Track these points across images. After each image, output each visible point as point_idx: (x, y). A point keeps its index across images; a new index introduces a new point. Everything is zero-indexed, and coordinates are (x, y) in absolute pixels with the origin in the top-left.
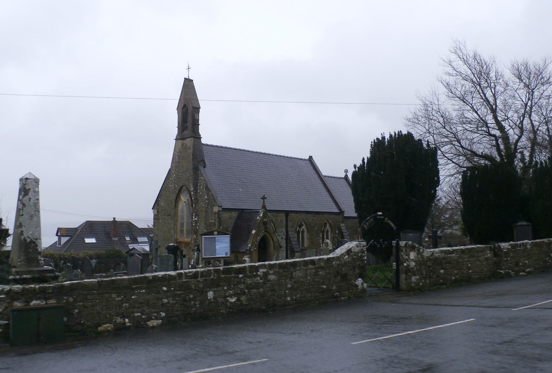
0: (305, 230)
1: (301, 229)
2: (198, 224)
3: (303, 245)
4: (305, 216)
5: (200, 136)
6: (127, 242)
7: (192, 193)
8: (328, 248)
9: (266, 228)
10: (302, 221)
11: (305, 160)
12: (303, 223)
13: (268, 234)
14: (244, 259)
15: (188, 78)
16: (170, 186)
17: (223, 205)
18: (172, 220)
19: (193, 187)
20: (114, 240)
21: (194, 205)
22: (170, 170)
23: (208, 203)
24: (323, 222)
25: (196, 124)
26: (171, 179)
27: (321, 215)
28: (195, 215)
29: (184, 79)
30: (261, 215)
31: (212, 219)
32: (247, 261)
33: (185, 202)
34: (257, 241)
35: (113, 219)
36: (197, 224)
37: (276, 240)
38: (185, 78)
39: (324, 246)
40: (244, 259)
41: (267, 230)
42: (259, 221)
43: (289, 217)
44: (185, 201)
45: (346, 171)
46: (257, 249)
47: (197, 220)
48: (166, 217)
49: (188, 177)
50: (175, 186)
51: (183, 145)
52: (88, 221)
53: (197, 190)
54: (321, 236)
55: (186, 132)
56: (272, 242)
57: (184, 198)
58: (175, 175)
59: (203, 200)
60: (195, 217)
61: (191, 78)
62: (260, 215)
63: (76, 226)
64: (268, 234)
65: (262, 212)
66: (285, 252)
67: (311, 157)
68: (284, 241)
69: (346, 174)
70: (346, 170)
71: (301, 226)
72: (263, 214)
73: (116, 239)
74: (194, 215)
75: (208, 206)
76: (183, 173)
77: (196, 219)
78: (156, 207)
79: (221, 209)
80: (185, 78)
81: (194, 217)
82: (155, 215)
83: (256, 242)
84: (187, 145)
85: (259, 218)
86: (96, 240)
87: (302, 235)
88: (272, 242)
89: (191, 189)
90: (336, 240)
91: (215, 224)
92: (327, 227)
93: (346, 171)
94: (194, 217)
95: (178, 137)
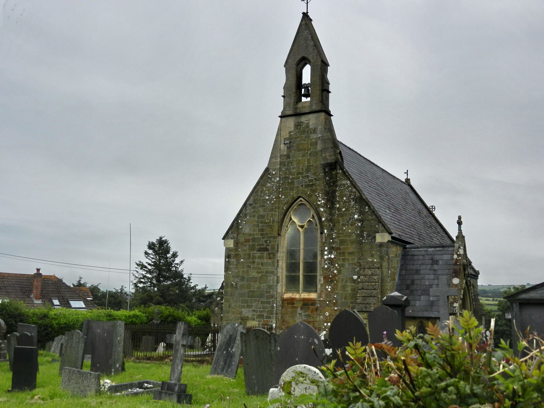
2: (337, 265)
6: (55, 307)
7: (322, 210)
18: (270, 258)
20: (36, 304)
22: (267, 170)
26: (269, 185)
35: (35, 272)
47: (334, 258)
53: (333, 204)
58: (278, 179)
60: (330, 253)
70: (432, 206)
73: (39, 302)
74: (326, 248)
75: (362, 232)
76: (299, 173)
81: (326, 253)
94: (326, 253)
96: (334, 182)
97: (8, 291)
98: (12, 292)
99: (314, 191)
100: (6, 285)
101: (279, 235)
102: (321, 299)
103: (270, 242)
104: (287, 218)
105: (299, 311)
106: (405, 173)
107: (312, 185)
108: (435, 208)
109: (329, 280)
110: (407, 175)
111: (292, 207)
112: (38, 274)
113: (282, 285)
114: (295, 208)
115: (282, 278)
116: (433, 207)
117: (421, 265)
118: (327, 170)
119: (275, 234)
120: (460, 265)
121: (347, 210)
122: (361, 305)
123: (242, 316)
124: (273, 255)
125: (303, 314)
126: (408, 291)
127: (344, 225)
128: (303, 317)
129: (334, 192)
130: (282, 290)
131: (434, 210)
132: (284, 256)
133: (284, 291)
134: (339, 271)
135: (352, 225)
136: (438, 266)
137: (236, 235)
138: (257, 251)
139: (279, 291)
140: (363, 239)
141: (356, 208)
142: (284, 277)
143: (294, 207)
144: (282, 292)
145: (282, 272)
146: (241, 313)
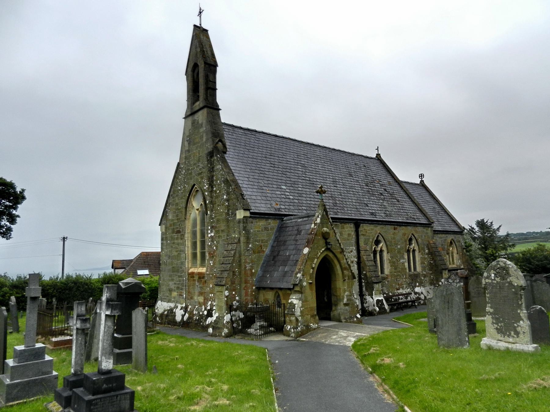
0: (384, 249)
1: (377, 247)
3: (382, 272)
4: (383, 227)
5: (218, 106)
8: (510, 283)
9: (327, 243)
10: (378, 235)
11: (372, 158)
12: (380, 238)
13: (331, 255)
14: (290, 301)
15: (199, 25)
16: (179, 188)
17: (252, 208)
19: (207, 184)
21: (209, 212)
22: (179, 164)
23: (228, 206)
24: (408, 237)
25: (211, 89)
27: (404, 227)
28: (210, 228)
29: (193, 27)
30: (319, 220)
31: (235, 232)
32: (296, 306)
33: (198, 210)
34: (313, 268)
36: (214, 243)
37: (347, 266)
38: (195, 26)
39: (493, 275)
40: (290, 301)
41: (329, 247)
42: (315, 231)
43: (360, 229)
44: (198, 208)
45: (421, 176)
46: (314, 283)
48: (175, 234)
49: (200, 169)
50: (184, 187)
51: (193, 123)
52: (143, 252)
53: (212, 188)
54: (406, 257)
55: (198, 104)
56: (338, 267)
57: (196, 203)
59: (220, 202)
60: (211, 232)
61: (204, 26)
62: (316, 220)
63: (132, 258)
64: (331, 255)
65: (320, 216)
66: (358, 284)
67: (378, 155)
68: (356, 266)
69: (422, 179)
70: (421, 174)
71: (377, 242)
72: (321, 219)
74: (209, 228)
75: (228, 211)
77: (213, 235)
78: (163, 222)
79: (248, 214)
80: (195, 26)
81: (209, 232)
82: (163, 234)
83: (312, 270)
84: (198, 122)
85: (314, 226)
86: (150, 272)
87: (380, 255)
88: (338, 267)
89: (205, 188)
90: (426, 262)
91: (239, 240)
92: (413, 245)
93: (421, 176)
94: (209, 232)
95: (189, 113)
96: (213, 168)
97: (149, 264)
98: (152, 264)
99: (202, 178)
100: (148, 260)
101: (185, 219)
102: (208, 273)
103: (181, 226)
104: (189, 204)
105: (197, 284)
106: (376, 149)
107: (201, 173)
108: (423, 176)
109: (212, 256)
110: (378, 151)
111: (191, 194)
112: (541, 231)
113: (188, 262)
114: (194, 194)
115: (188, 255)
116: (422, 175)
117: (289, 237)
118: (209, 158)
119: (184, 219)
120: (313, 234)
121: (220, 192)
122: (219, 279)
123: (170, 288)
124: (182, 237)
125: (199, 286)
126: (273, 261)
127: (218, 205)
128: (199, 289)
129: (213, 176)
130: (188, 265)
131: (423, 177)
132: (189, 237)
133: (190, 266)
134: (217, 247)
135: (223, 205)
136: (300, 236)
137: (165, 222)
138: (176, 234)
139: (186, 266)
140: (229, 217)
141: (225, 189)
142: (190, 255)
143: (193, 194)
144: (188, 267)
145: (189, 251)
146: (169, 285)
